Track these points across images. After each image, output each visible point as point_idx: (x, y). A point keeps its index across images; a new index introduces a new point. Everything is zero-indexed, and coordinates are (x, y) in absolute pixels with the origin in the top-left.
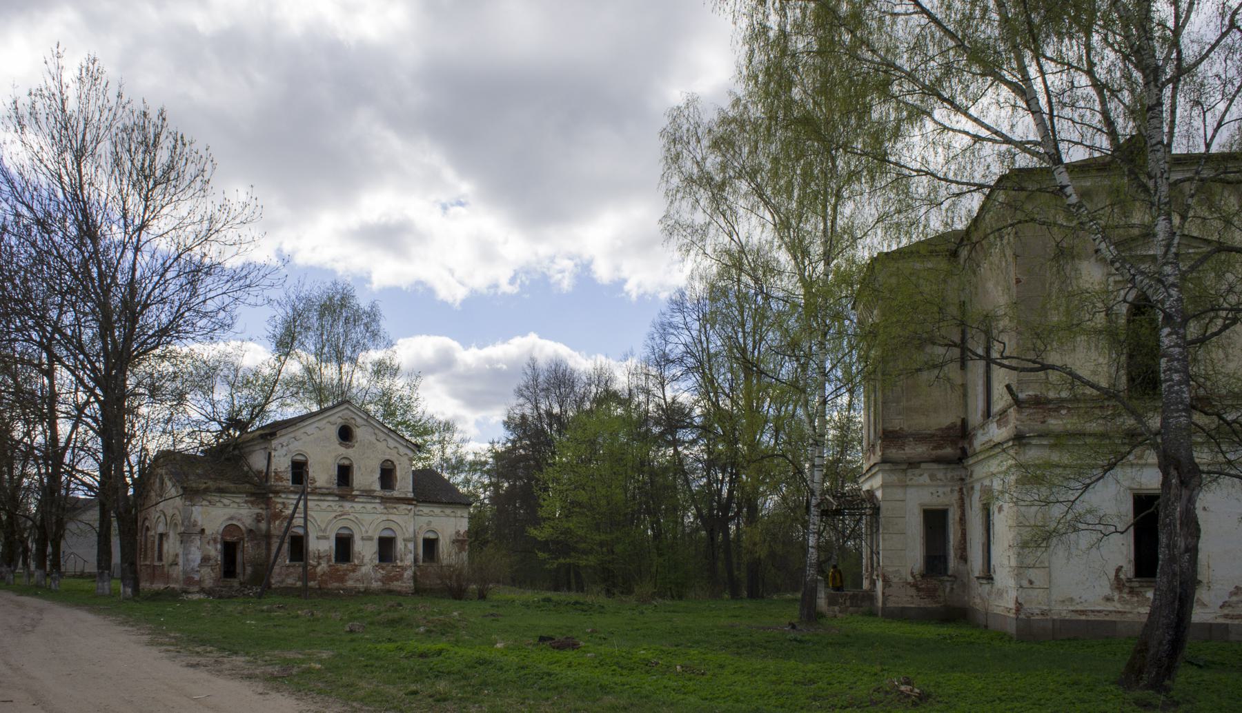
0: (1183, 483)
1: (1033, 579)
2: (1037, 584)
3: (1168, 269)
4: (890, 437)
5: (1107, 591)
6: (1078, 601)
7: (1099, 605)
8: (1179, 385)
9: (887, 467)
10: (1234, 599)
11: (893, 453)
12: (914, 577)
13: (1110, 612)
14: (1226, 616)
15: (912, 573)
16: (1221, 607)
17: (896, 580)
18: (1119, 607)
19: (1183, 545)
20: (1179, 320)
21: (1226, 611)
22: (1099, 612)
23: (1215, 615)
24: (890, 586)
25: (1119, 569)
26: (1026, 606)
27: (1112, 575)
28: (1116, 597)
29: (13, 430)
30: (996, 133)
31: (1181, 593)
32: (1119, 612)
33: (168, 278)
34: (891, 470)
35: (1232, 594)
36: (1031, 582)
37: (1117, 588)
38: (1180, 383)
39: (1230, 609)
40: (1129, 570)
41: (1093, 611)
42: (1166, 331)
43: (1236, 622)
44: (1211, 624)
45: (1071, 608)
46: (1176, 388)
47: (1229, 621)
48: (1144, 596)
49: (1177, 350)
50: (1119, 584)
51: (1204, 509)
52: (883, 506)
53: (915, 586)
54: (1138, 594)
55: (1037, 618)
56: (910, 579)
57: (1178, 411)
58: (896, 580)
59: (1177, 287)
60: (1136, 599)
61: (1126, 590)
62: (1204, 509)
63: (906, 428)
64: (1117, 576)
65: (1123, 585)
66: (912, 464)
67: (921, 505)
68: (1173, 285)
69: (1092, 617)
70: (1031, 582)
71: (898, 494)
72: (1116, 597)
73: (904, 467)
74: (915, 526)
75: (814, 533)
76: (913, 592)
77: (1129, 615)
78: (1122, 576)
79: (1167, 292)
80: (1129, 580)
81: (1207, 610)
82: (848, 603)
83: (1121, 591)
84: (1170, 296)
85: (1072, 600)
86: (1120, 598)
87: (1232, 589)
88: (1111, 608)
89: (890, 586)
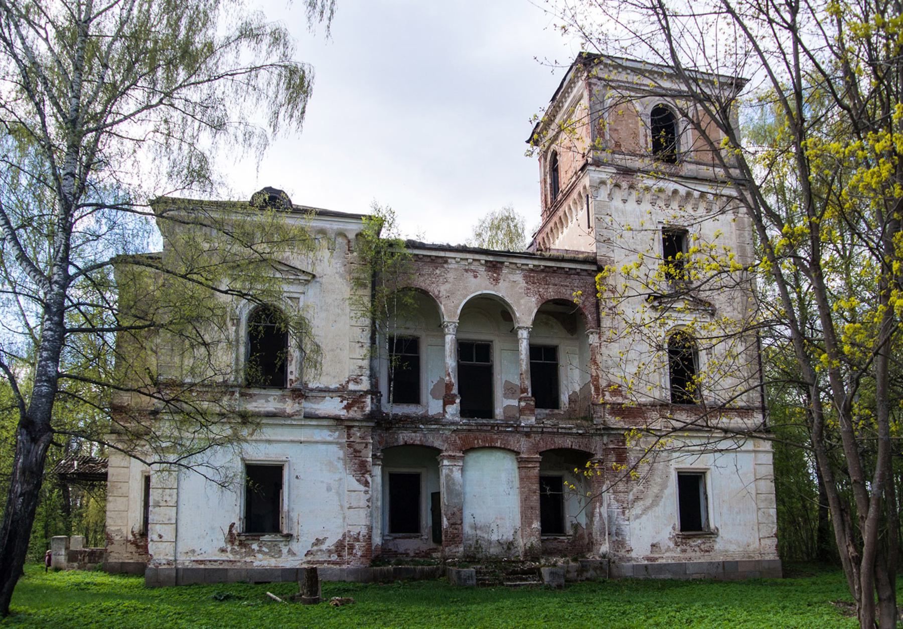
1: (162, 534)
2: (165, 538)
5: (222, 544)
6: (199, 552)
7: (215, 555)
8: (45, 361)
10: (315, 548)
12: (134, 535)
13: (224, 561)
14: (309, 562)
15: (132, 532)
16: (306, 555)
17: (118, 538)
18: (231, 557)
19: (19, 490)
20: (55, 310)
21: (309, 558)
22: (215, 561)
23: (301, 562)
24: (112, 543)
27: (227, 531)
28: (229, 549)
30: (758, 220)
31: (11, 531)
32: (231, 561)
35: (314, 544)
36: (160, 537)
37: (230, 541)
39: (312, 556)
40: (239, 528)
41: (210, 561)
44: (297, 569)
45: (193, 559)
46: (43, 363)
48: (250, 547)
49: (50, 333)
50: (231, 538)
51: (297, 477)
53: (134, 543)
55: (164, 567)
56: (131, 537)
58: (118, 538)
59: (58, 284)
60: (244, 550)
61: (237, 543)
62: (297, 477)
63: (133, 404)
64: (230, 531)
65: (235, 538)
67: (142, 472)
68: (56, 282)
69: (209, 566)
70: (160, 537)
72: (229, 549)
76: (132, 548)
77: (238, 564)
78: (234, 531)
79: (51, 287)
81: (296, 558)
82: (86, 560)
83: (233, 544)
84: (52, 290)
85: (193, 551)
87: (314, 541)
88: (226, 559)
89: (112, 543)
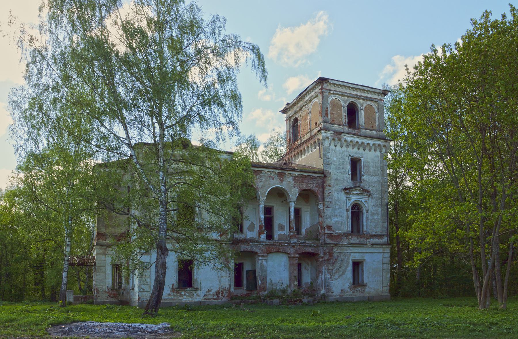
0: (163, 254)
2: (146, 290)
3: (162, 187)
4: (100, 235)
9: (98, 247)
11: (101, 241)
12: (108, 289)
14: (205, 299)
15: (108, 288)
18: (173, 297)
21: (205, 298)
22: (166, 299)
24: (99, 293)
25: (173, 285)
26: (141, 298)
27: (171, 287)
28: (172, 294)
29: (475, 322)
33: (241, 45)
34: (100, 248)
35: (207, 292)
36: (143, 289)
38: (163, 223)
40: (176, 285)
42: (161, 206)
43: (208, 301)
47: (206, 301)
49: (163, 213)
52: (97, 262)
54: (179, 293)
56: (107, 290)
57: (162, 231)
58: (101, 291)
61: (175, 292)
63: (106, 233)
64: (172, 287)
66: (108, 246)
68: (163, 192)
71: (103, 257)
72: (172, 294)
73: (105, 247)
74: (109, 270)
75: (66, 271)
80: (176, 288)
86: (173, 294)
89: (99, 293)
